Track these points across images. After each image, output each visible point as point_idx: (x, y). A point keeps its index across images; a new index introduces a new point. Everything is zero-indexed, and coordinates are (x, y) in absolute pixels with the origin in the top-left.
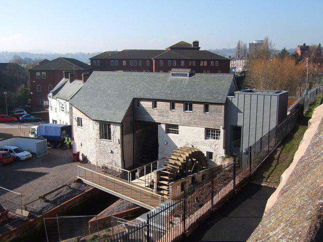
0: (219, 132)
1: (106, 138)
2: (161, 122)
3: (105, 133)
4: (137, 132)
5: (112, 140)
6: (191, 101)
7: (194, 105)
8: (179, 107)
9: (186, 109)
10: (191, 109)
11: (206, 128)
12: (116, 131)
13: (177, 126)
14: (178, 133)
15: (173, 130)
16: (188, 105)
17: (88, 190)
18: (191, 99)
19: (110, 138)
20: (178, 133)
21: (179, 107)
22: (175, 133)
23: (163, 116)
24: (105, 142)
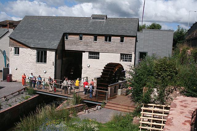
0: (131, 56)
1: (41, 62)
2: (85, 50)
3: (41, 57)
4: (64, 59)
5: (94, 41)
6: (123, 35)
7: (112, 38)
8: (101, 39)
9: (106, 40)
10: (110, 40)
11: (121, 54)
12: (51, 56)
13: (98, 53)
14: (99, 59)
15: (94, 57)
16: (108, 38)
17: (14, 106)
18: (110, 33)
19: (45, 62)
20: (99, 59)
21: (101, 39)
22: (96, 59)
23: (87, 45)
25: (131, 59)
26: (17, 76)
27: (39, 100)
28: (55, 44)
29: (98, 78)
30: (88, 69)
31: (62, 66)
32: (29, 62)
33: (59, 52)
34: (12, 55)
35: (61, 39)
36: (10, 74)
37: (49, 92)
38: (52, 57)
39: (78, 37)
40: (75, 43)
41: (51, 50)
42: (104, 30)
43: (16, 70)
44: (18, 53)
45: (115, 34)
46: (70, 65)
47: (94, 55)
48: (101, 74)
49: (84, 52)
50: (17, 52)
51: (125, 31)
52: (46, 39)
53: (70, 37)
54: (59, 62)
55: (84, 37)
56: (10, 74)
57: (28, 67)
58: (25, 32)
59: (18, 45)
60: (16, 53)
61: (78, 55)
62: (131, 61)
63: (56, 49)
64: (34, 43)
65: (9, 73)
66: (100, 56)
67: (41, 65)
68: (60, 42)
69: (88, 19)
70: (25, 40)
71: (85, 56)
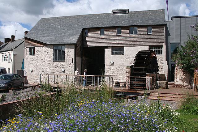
0: (162, 48)
3: (59, 55)
11: (149, 46)
12: (70, 53)
13: (122, 48)
19: (63, 59)
22: (121, 54)
24: (60, 63)
25: (161, 51)
26: (33, 79)
27: (52, 100)
28: (74, 39)
29: (131, 67)
30: (112, 67)
31: (82, 65)
32: (46, 61)
33: (78, 48)
34: (27, 56)
35: (81, 34)
36: (25, 75)
37: (5, 52)
38: (71, 53)
39: (98, 33)
40: (96, 39)
41: (69, 45)
42: (125, 24)
43: (32, 71)
44: (34, 54)
45: (141, 25)
46: (91, 61)
47: (118, 50)
48: (134, 62)
49: (106, 47)
50: (32, 52)
51: (152, 21)
52: (64, 36)
53: (90, 34)
54: (79, 59)
55: (106, 32)
56: (25, 75)
57: (44, 67)
58: (41, 32)
59: (33, 44)
60: (31, 54)
61: (100, 51)
62: (161, 54)
63: (75, 43)
64: (50, 40)
65: (24, 75)
66: (124, 51)
67: (58, 64)
68: (79, 38)
69: (108, 15)
70: (40, 38)
71: (108, 52)
